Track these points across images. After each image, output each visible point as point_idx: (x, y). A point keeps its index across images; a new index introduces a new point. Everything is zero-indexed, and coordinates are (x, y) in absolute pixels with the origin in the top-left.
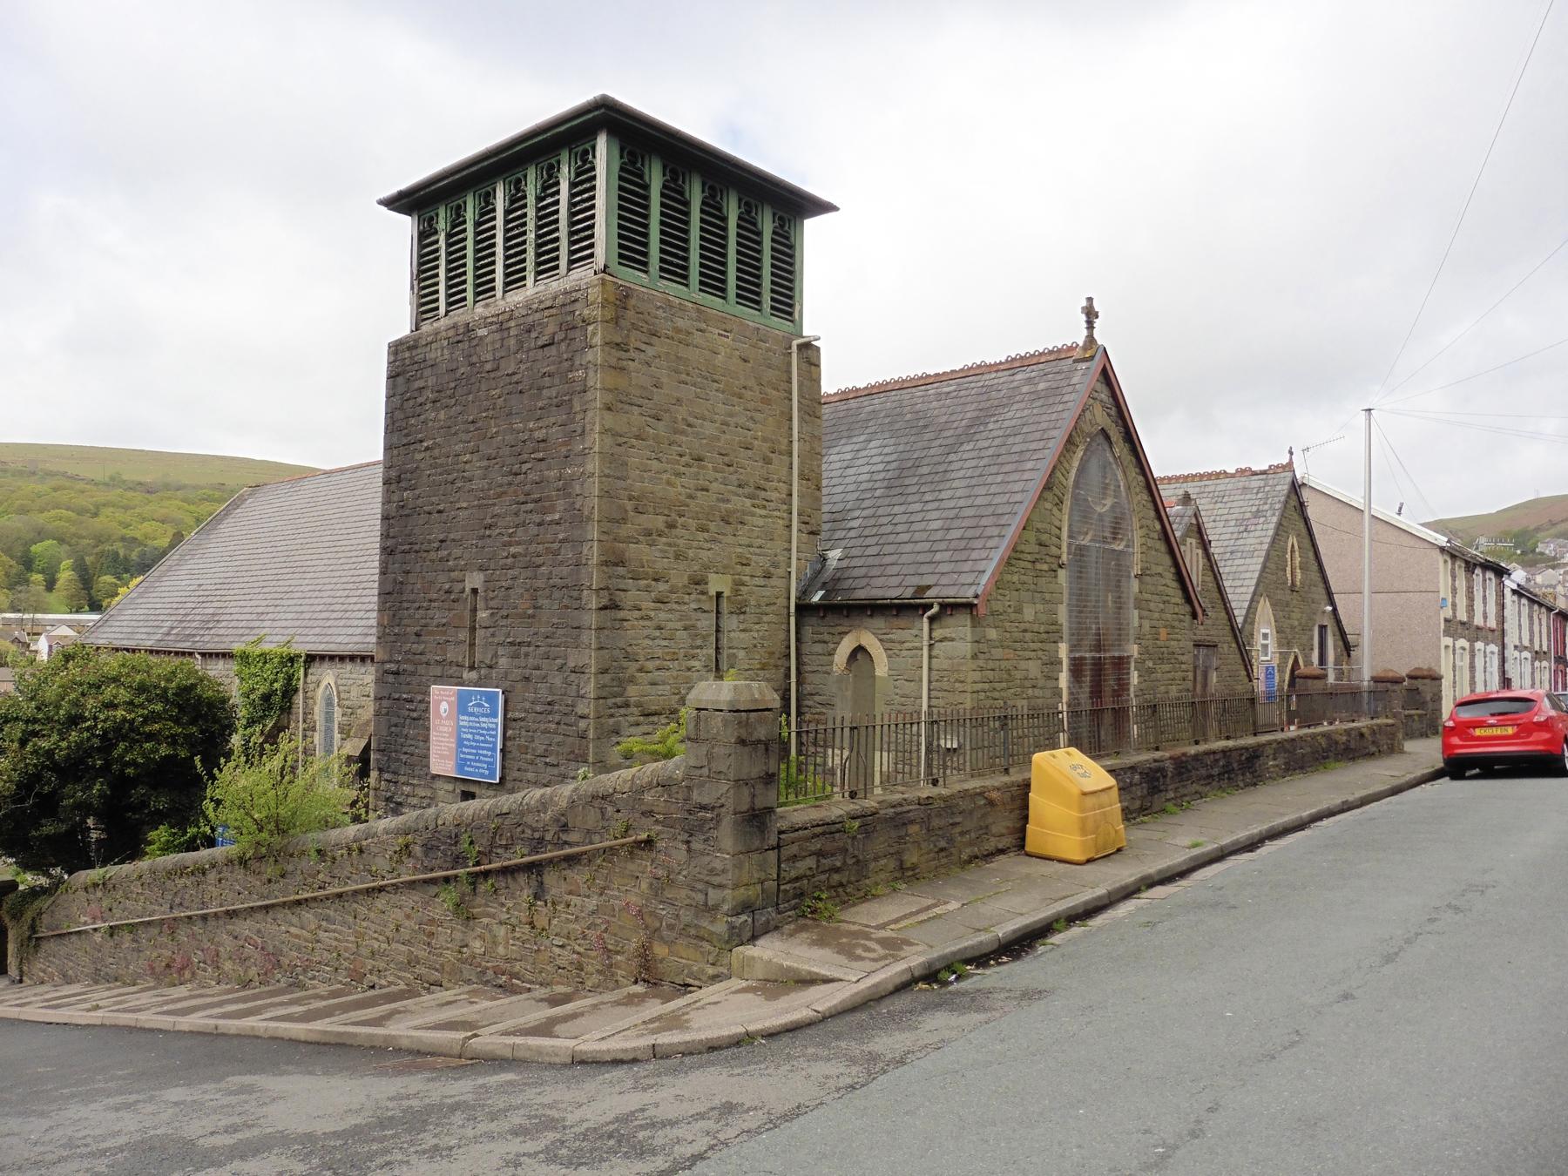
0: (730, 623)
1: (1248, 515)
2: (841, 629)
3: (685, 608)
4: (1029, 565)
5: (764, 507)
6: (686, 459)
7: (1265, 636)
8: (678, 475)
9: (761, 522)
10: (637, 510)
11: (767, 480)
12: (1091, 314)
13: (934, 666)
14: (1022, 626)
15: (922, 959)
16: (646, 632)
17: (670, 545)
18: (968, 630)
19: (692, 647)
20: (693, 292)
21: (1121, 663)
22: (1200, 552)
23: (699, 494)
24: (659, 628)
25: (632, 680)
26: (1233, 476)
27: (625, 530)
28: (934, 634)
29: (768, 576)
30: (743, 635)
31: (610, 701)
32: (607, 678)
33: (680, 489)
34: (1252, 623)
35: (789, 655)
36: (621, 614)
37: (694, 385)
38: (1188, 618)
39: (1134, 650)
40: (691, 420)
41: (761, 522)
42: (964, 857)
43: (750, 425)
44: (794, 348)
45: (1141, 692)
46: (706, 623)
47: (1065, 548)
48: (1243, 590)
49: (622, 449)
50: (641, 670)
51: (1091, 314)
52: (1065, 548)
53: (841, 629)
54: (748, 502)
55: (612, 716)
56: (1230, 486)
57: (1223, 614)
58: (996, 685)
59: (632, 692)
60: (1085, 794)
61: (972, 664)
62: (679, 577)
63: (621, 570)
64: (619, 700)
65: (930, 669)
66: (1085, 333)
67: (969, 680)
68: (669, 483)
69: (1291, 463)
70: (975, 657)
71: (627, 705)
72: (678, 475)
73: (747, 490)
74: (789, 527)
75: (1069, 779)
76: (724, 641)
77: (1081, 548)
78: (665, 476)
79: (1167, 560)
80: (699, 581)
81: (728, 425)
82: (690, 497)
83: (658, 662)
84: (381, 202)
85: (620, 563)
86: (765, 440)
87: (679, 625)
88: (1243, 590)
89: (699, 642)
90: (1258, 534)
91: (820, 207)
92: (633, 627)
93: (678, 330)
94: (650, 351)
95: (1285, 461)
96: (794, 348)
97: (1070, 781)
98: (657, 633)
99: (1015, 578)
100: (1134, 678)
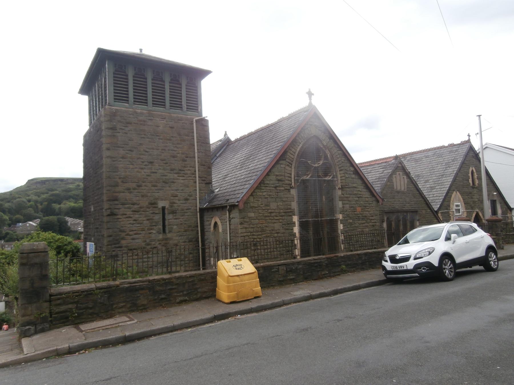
0: (168, 217)
1: (451, 161)
2: (211, 216)
3: (147, 213)
4: (273, 189)
5: (183, 176)
6: (145, 163)
7: (457, 206)
8: (142, 169)
9: (182, 181)
10: (122, 182)
11: (185, 167)
12: (310, 94)
13: (231, 228)
14: (270, 211)
15: (77, 344)
16: (129, 222)
17: (139, 192)
18: (238, 214)
19: (151, 226)
20: (150, 107)
21: (333, 223)
22: (405, 177)
23: (152, 174)
24: (135, 220)
25: (123, 239)
26: (447, 147)
27: (118, 189)
28: (231, 216)
29: (187, 199)
30: (175, 220)
31: (113, 246)
32: (111, 238)
33: (143, 173)
34: (449, 201)
35: (197, 226)
36: (118, 217)
37: (148, 138)
38: (374, 203)
39: (340, 216)
40: (147, 150)
41: (182, 181)
42: (178, 301)
43: (175, 149)
44: (194, 121)
45: (344, 232)
46: (158, 217)
47: (293, 181)
48: (444, 189)
49: (114, 162)
50: (127, 235)
51: (310, 94)
52: (293, 181)
53: (211, 216)
54: (176, 175)
55: (114, 251)
56: (445, 151)
57: (421, 199)
58: (254, 233)
59: (124, 242)
60: (230, 276)
61: (240, 226)
62: (144, 203)
63: (116, 202)
64: (117, 245)
65: (230, 229)
66: (309, 101)
67: (239, 232)
68: (138, 172)
69: (469, 140)
70: (241, 224)
71: (121, 247)
72: (142, 169)
73: (175, 171)
74: (196, 182)
75: (236, 270)
76: (167, 223)
77: (304, 182)
78: (136, 170)
79: (359, 182)
80: (153, 204)
81: (164, 150)
82: (148, 176)
83: (135, 232)
84: (310, 89)
85: (116, 200)
86: (183, 154)
87: (145, 219)
88: (444, 189)
89: (154, 224)
90: (453, 168)
91: (202, 73)
92: (123, 221)
93: (141, 121)
94: (127, 129)
95: (467, 139)
96: (194, 121)
97: (236, 270)
98: (135, 222)
99: (264, 194)
100: (341, 227)
